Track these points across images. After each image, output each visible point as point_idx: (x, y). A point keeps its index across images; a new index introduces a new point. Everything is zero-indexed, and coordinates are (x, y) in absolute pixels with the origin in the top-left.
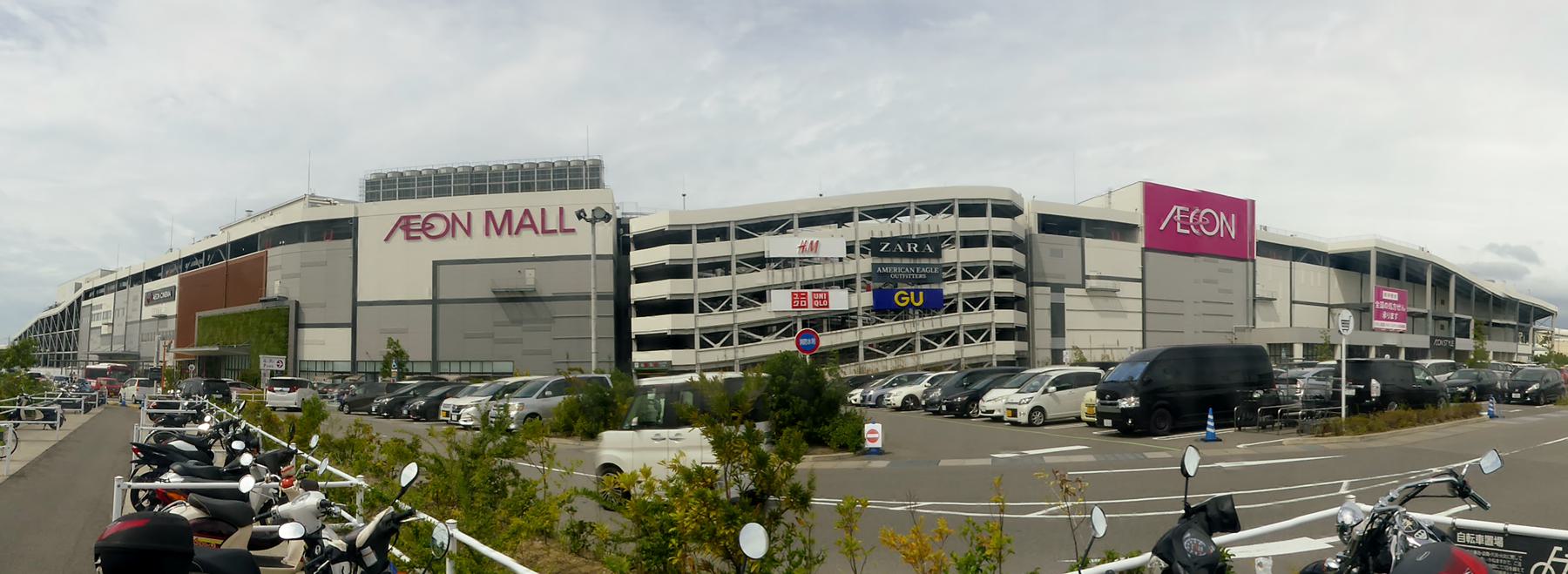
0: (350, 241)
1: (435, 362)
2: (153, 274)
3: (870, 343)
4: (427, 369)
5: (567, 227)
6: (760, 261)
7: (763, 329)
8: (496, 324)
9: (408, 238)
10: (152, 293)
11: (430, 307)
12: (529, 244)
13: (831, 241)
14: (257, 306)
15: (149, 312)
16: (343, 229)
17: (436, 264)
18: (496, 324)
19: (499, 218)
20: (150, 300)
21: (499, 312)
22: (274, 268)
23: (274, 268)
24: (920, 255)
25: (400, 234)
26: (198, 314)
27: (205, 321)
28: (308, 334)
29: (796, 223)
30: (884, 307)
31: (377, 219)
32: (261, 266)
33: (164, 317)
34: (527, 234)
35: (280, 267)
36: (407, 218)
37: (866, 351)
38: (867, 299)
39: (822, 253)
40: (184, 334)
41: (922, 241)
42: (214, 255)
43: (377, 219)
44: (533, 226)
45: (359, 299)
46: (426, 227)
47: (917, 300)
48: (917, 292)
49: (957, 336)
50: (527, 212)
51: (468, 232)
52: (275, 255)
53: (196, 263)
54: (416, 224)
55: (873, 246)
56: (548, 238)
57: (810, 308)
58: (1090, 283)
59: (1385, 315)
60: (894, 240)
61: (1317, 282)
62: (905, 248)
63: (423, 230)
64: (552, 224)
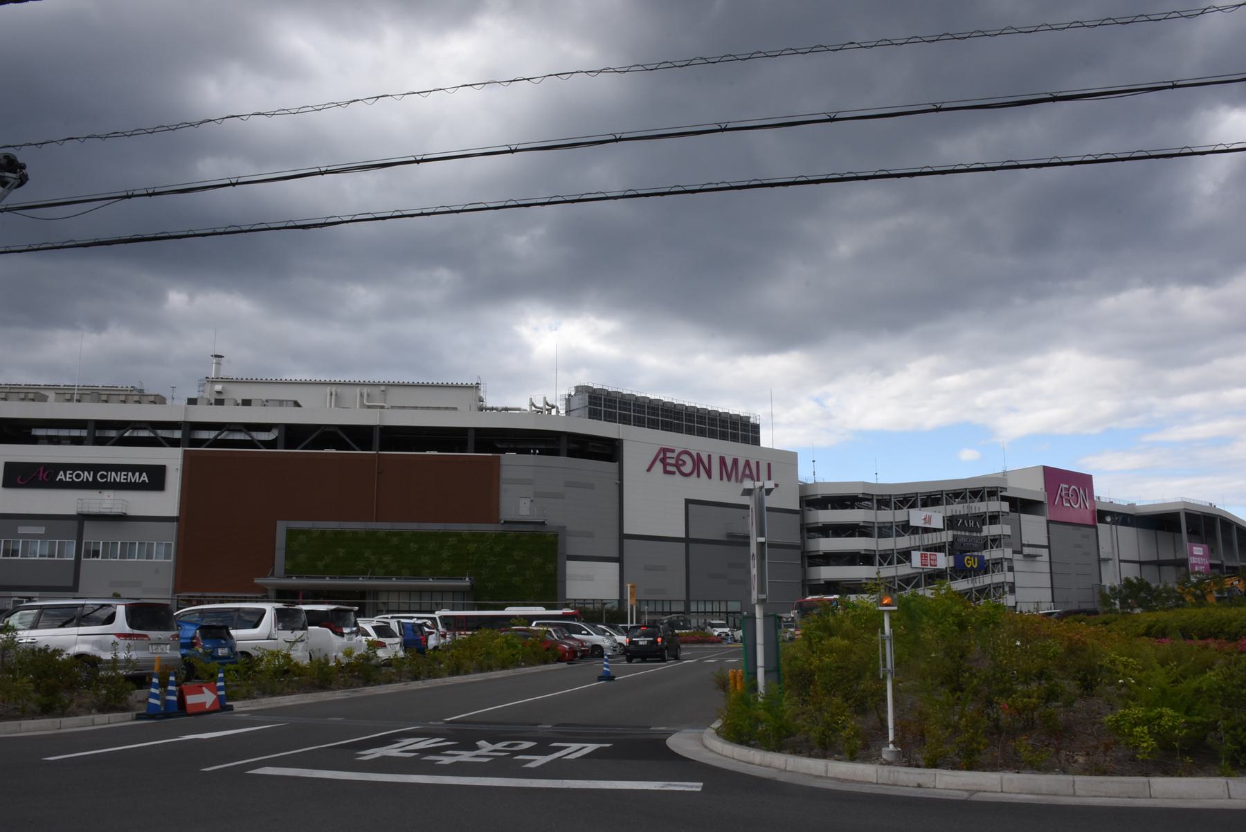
6: (906, 528)
9: (666, 472)
11: (692, 546)
13: (935, 516)
17: (688, 502)
19: (729, 463)
25: (659, 466)
36: (665, 450)
39: (932, 526)
42: (294, 434)
58: (1026, 550)
61: (1128, 535)
63: (677, 466)
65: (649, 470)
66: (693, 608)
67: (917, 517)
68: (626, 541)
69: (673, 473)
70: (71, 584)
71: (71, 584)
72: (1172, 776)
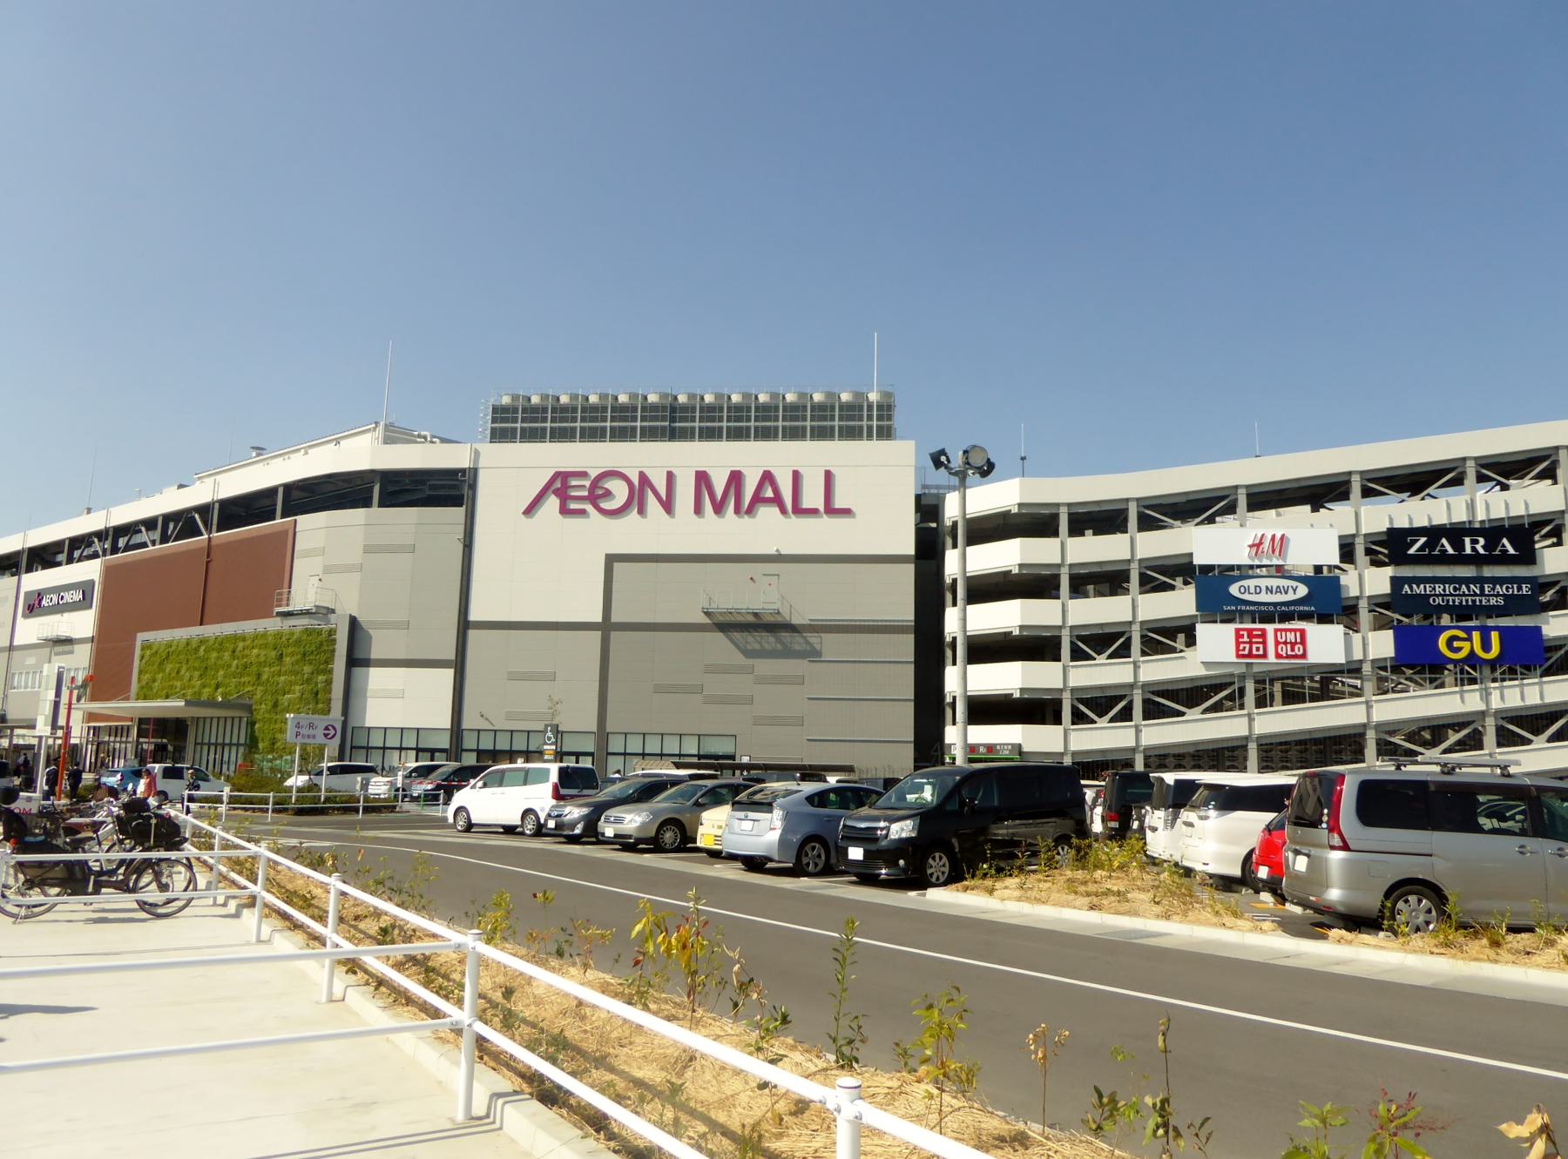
0: (458, 513)
1: (602, 735)
2: (43, 557)
3: (1390, 728)
4: (589, 745)
5: (839, 503)
7: (1191, 695)
8: (710, 669)
10: (40, 595)
12: (768, 531)
13: (1311, 539)
14: (272, 625)
15: (31, 630)
16: (447, 490)
17: (611, 560)
18: (710, 669)
20: (35, 605)
21: (720, 647)
22: (308, 554)
23: (308, 554)
24: (1490, 560)
25: (553, 502)
26: (141, 637)
27: (162, 657)
28: (376, 678)
29: (1242, 502)
30: (1418, 661)
31: (510, 473)
32: (283, 546)
33: (68, 641)
34: (768, 513)
35: (322, 551)
37: (1146, 702)
38: (1382, 645)
40: (106, 677)
41: (1493, 532)
43: (510, 473)
44: (777, 500)
45: (475, 615)
46: (596, 494)
47: (1486, 646)
48: (1485, 633)
49: (1242, 691)
50: (768, 477)
51: (668, 505)
52: (314, 530)
53: (144, 536)
54: (580, 488)
55: (1392, 547)
56: (795, 521)
57: (1272, 658)
59: (78, 596)
60: (1434, 533)
62: (1458, 546)
63: (593, 498)
64: (813, 496)
65: (514, 677)
66: (616, 745)
67: (1211, 544)
68: (451, 655)
69: (582, 512)
70: (617, 566)
71: (617, 566)
72: (1114, 533)
